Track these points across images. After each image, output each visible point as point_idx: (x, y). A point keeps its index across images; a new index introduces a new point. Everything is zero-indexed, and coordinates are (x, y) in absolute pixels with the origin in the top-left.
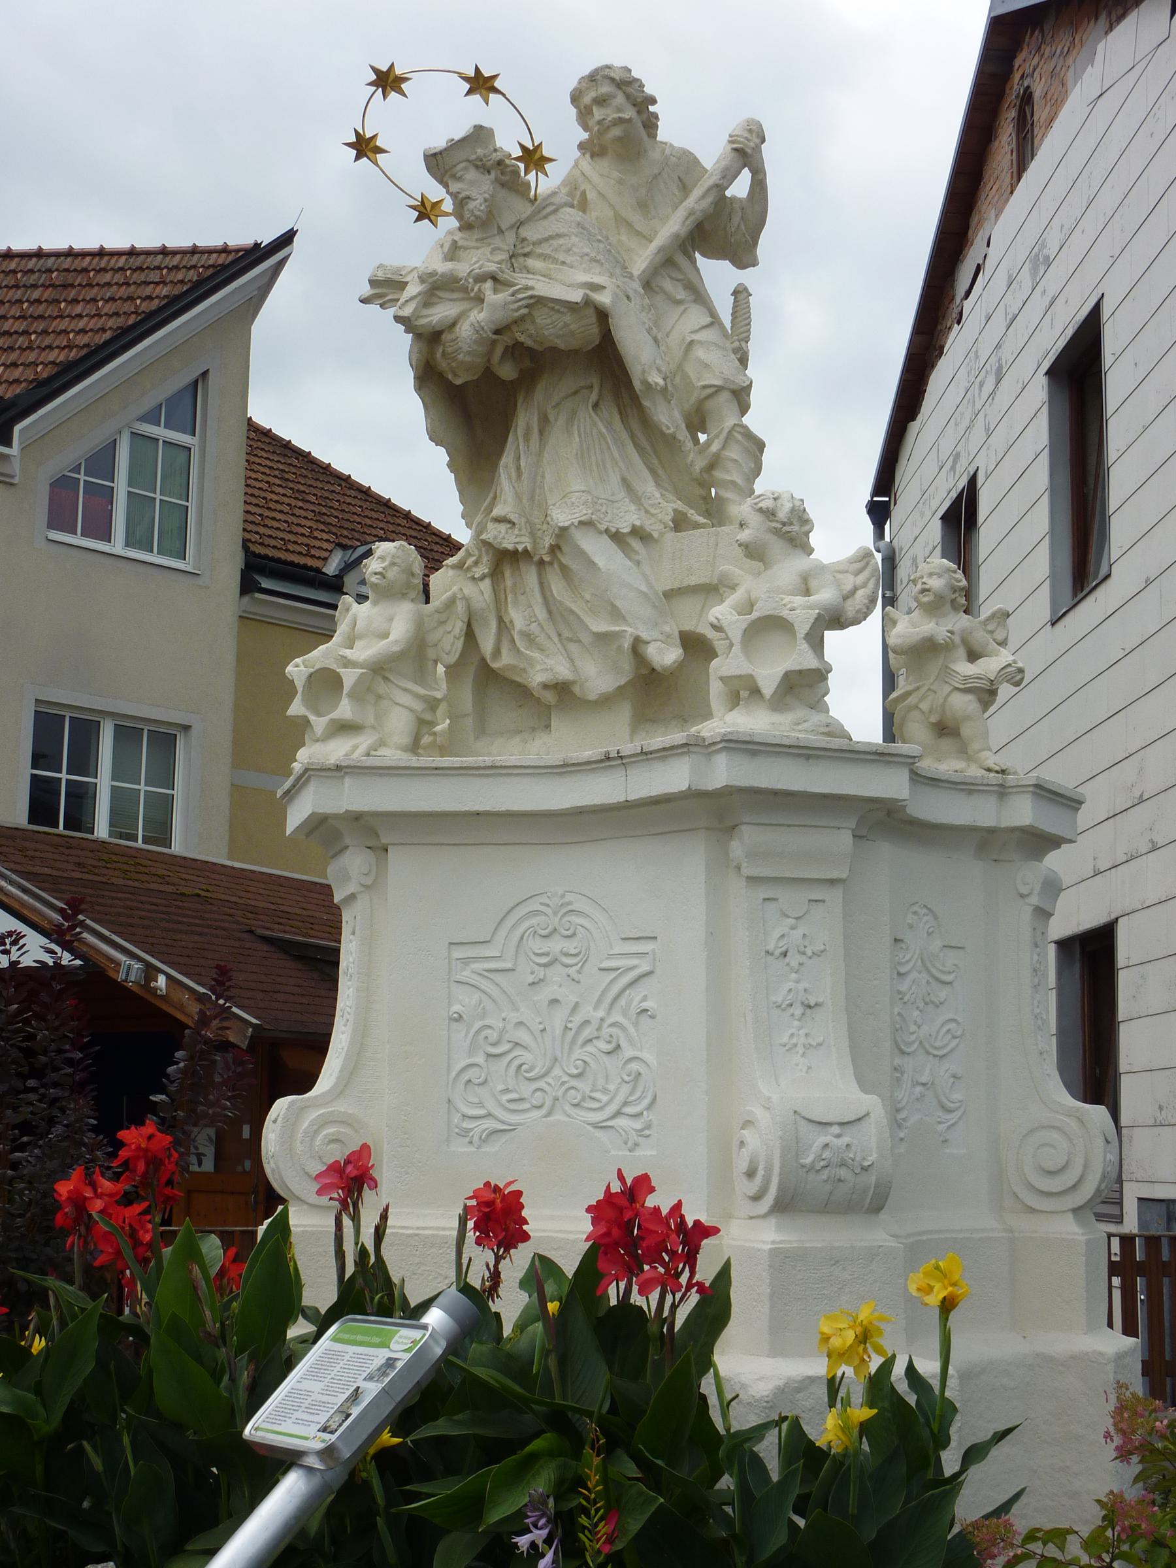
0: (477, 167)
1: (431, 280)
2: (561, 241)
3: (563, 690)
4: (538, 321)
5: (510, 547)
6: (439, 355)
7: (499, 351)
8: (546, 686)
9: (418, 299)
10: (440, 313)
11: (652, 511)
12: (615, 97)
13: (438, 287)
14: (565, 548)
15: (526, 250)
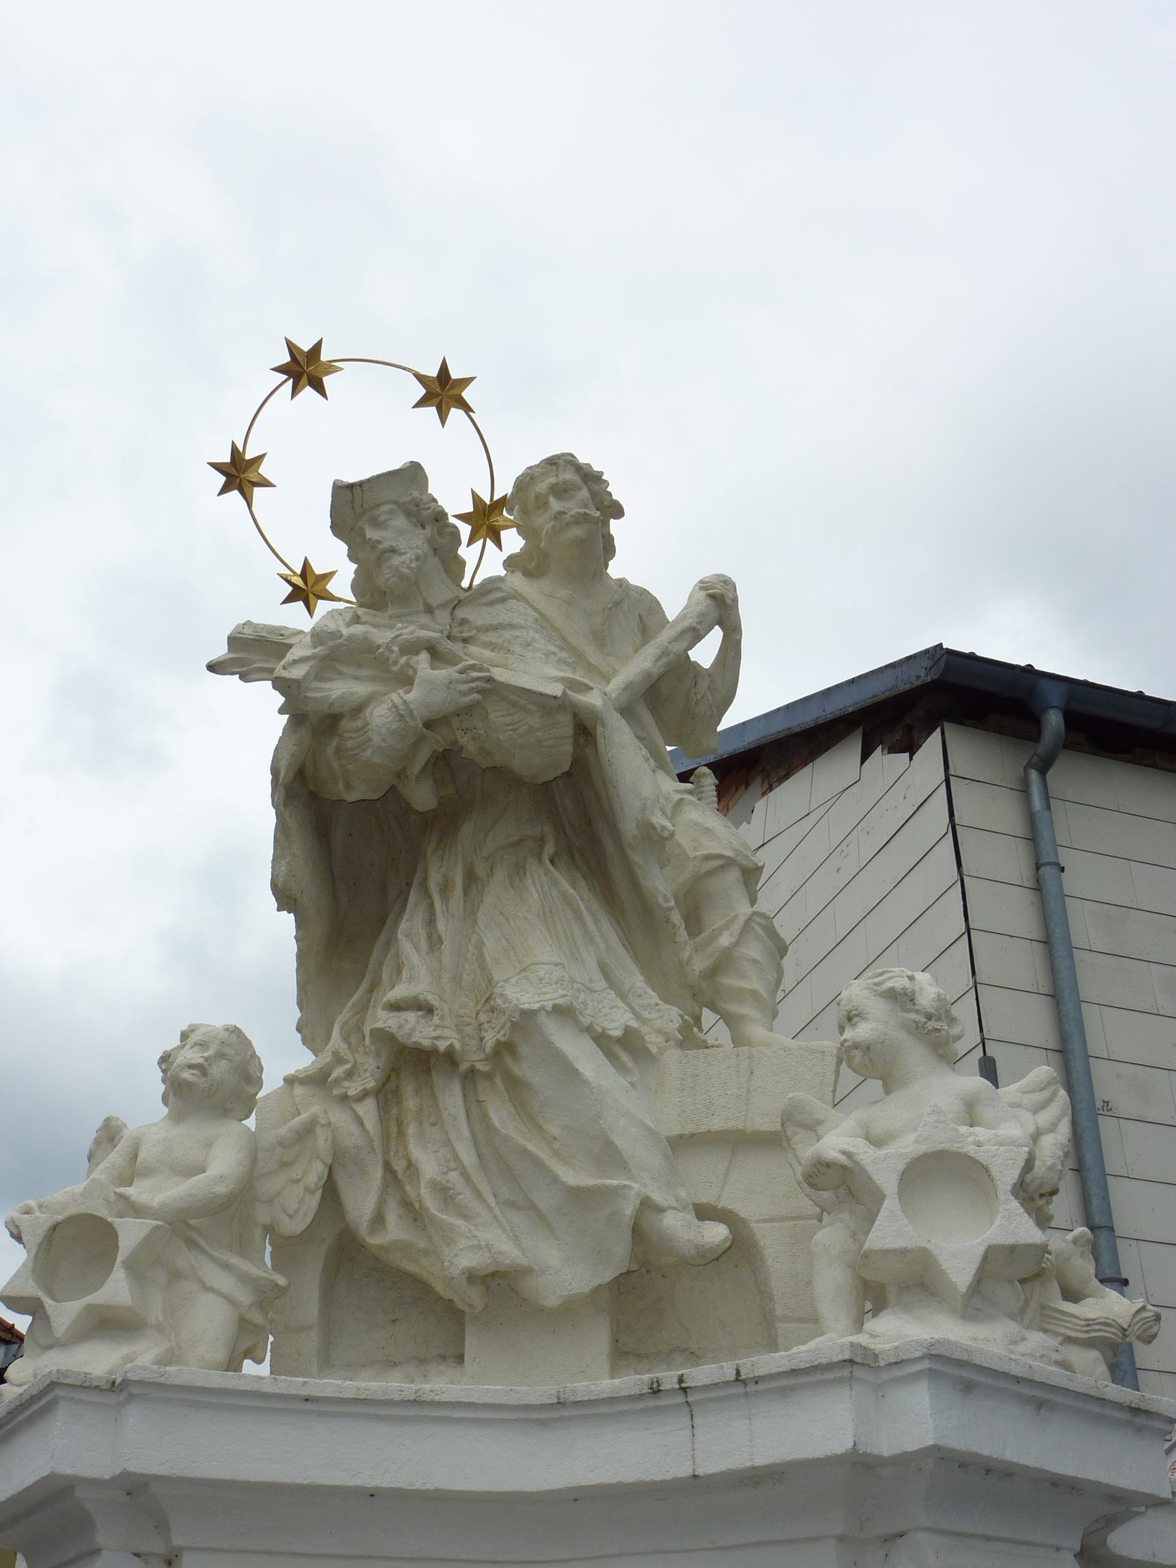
1: (330, 643)
2: (516, 633)
3: (501, 1286)
4: (492, 716)
5: (426, 1043)
6: (330, 750)
7: (424, 755)
8: (472, 1277)
9: (310, 663)
10: (341, 689)
11: (645, 1014)
12: (580, 489)
14: (524, 1050)
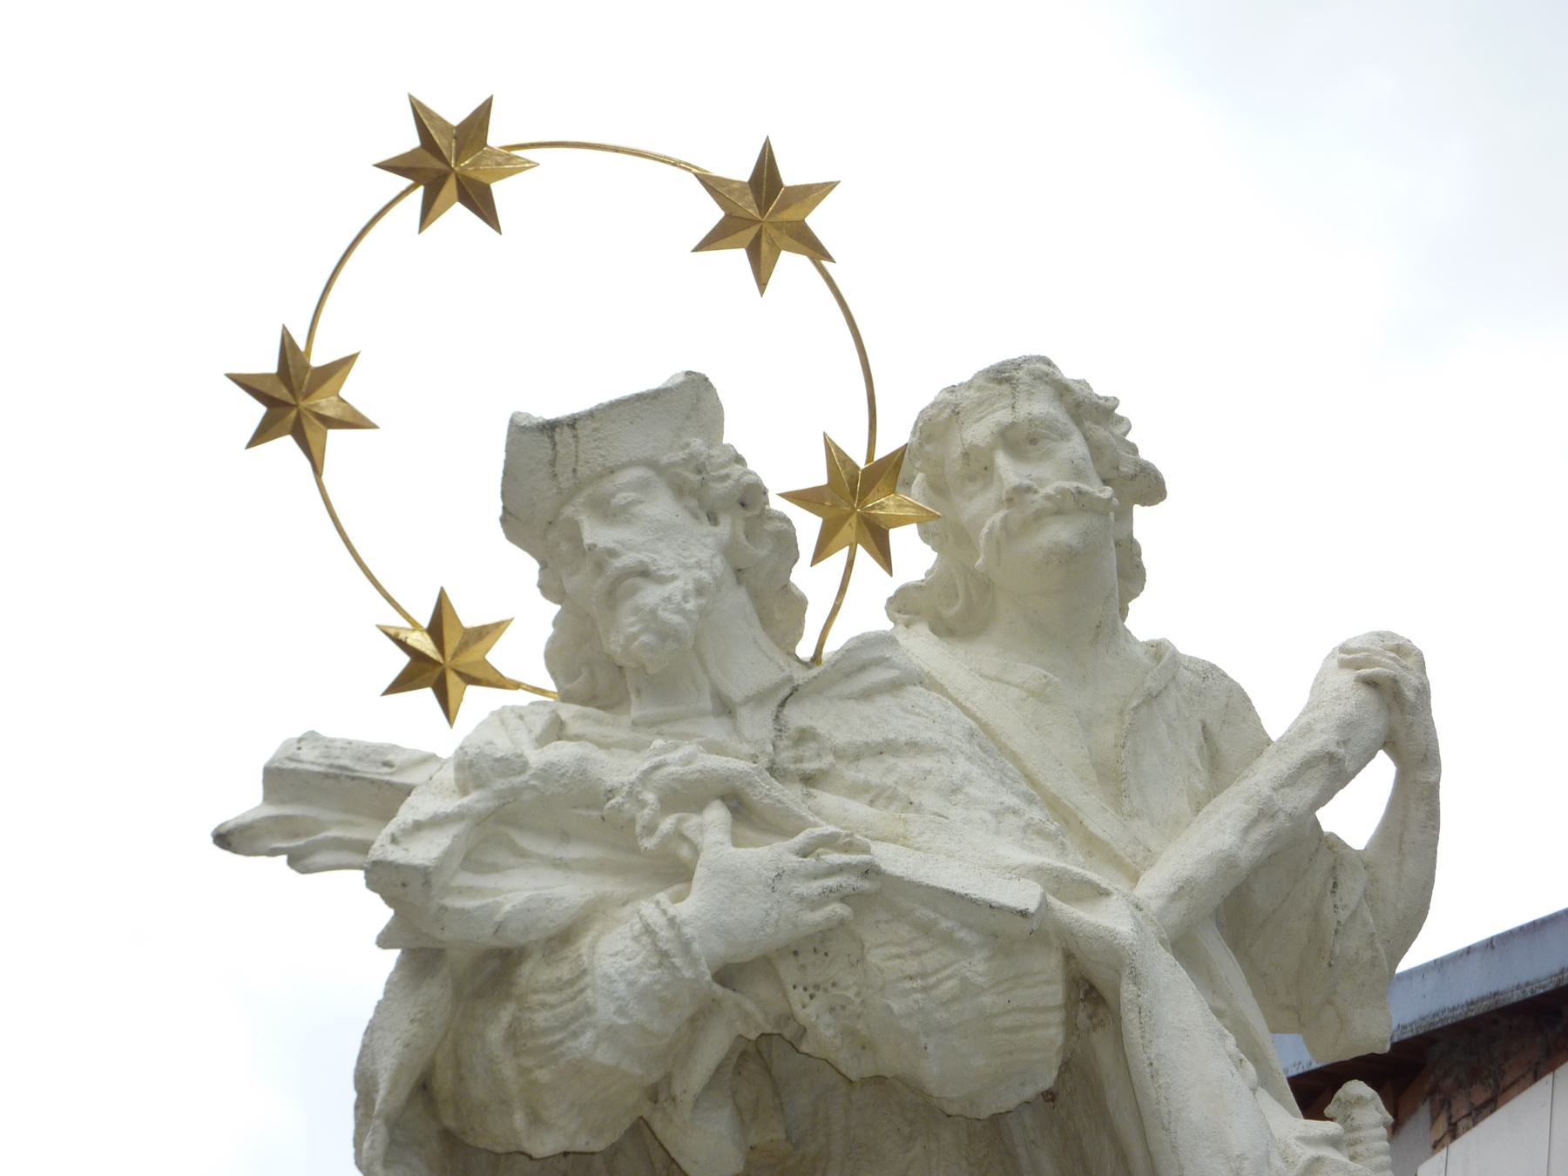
0: (680, 490)
1: (500, 784)
2: (926, 763)
4: (874, 957)
6: (495, 1034)
7: (714, 1047)
10: (521, 891)
12: (1064, 436)
13: (512, 808)
15: (810, 766)
